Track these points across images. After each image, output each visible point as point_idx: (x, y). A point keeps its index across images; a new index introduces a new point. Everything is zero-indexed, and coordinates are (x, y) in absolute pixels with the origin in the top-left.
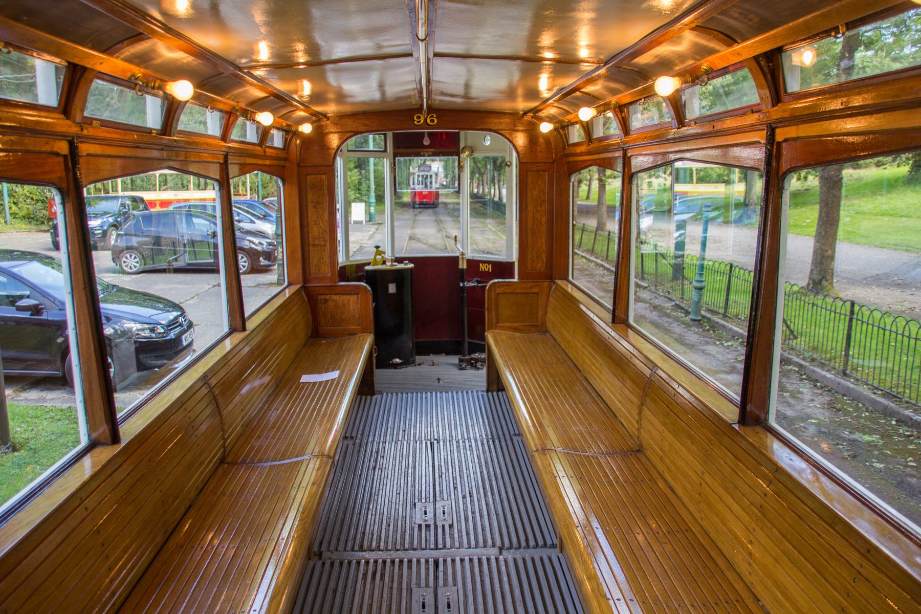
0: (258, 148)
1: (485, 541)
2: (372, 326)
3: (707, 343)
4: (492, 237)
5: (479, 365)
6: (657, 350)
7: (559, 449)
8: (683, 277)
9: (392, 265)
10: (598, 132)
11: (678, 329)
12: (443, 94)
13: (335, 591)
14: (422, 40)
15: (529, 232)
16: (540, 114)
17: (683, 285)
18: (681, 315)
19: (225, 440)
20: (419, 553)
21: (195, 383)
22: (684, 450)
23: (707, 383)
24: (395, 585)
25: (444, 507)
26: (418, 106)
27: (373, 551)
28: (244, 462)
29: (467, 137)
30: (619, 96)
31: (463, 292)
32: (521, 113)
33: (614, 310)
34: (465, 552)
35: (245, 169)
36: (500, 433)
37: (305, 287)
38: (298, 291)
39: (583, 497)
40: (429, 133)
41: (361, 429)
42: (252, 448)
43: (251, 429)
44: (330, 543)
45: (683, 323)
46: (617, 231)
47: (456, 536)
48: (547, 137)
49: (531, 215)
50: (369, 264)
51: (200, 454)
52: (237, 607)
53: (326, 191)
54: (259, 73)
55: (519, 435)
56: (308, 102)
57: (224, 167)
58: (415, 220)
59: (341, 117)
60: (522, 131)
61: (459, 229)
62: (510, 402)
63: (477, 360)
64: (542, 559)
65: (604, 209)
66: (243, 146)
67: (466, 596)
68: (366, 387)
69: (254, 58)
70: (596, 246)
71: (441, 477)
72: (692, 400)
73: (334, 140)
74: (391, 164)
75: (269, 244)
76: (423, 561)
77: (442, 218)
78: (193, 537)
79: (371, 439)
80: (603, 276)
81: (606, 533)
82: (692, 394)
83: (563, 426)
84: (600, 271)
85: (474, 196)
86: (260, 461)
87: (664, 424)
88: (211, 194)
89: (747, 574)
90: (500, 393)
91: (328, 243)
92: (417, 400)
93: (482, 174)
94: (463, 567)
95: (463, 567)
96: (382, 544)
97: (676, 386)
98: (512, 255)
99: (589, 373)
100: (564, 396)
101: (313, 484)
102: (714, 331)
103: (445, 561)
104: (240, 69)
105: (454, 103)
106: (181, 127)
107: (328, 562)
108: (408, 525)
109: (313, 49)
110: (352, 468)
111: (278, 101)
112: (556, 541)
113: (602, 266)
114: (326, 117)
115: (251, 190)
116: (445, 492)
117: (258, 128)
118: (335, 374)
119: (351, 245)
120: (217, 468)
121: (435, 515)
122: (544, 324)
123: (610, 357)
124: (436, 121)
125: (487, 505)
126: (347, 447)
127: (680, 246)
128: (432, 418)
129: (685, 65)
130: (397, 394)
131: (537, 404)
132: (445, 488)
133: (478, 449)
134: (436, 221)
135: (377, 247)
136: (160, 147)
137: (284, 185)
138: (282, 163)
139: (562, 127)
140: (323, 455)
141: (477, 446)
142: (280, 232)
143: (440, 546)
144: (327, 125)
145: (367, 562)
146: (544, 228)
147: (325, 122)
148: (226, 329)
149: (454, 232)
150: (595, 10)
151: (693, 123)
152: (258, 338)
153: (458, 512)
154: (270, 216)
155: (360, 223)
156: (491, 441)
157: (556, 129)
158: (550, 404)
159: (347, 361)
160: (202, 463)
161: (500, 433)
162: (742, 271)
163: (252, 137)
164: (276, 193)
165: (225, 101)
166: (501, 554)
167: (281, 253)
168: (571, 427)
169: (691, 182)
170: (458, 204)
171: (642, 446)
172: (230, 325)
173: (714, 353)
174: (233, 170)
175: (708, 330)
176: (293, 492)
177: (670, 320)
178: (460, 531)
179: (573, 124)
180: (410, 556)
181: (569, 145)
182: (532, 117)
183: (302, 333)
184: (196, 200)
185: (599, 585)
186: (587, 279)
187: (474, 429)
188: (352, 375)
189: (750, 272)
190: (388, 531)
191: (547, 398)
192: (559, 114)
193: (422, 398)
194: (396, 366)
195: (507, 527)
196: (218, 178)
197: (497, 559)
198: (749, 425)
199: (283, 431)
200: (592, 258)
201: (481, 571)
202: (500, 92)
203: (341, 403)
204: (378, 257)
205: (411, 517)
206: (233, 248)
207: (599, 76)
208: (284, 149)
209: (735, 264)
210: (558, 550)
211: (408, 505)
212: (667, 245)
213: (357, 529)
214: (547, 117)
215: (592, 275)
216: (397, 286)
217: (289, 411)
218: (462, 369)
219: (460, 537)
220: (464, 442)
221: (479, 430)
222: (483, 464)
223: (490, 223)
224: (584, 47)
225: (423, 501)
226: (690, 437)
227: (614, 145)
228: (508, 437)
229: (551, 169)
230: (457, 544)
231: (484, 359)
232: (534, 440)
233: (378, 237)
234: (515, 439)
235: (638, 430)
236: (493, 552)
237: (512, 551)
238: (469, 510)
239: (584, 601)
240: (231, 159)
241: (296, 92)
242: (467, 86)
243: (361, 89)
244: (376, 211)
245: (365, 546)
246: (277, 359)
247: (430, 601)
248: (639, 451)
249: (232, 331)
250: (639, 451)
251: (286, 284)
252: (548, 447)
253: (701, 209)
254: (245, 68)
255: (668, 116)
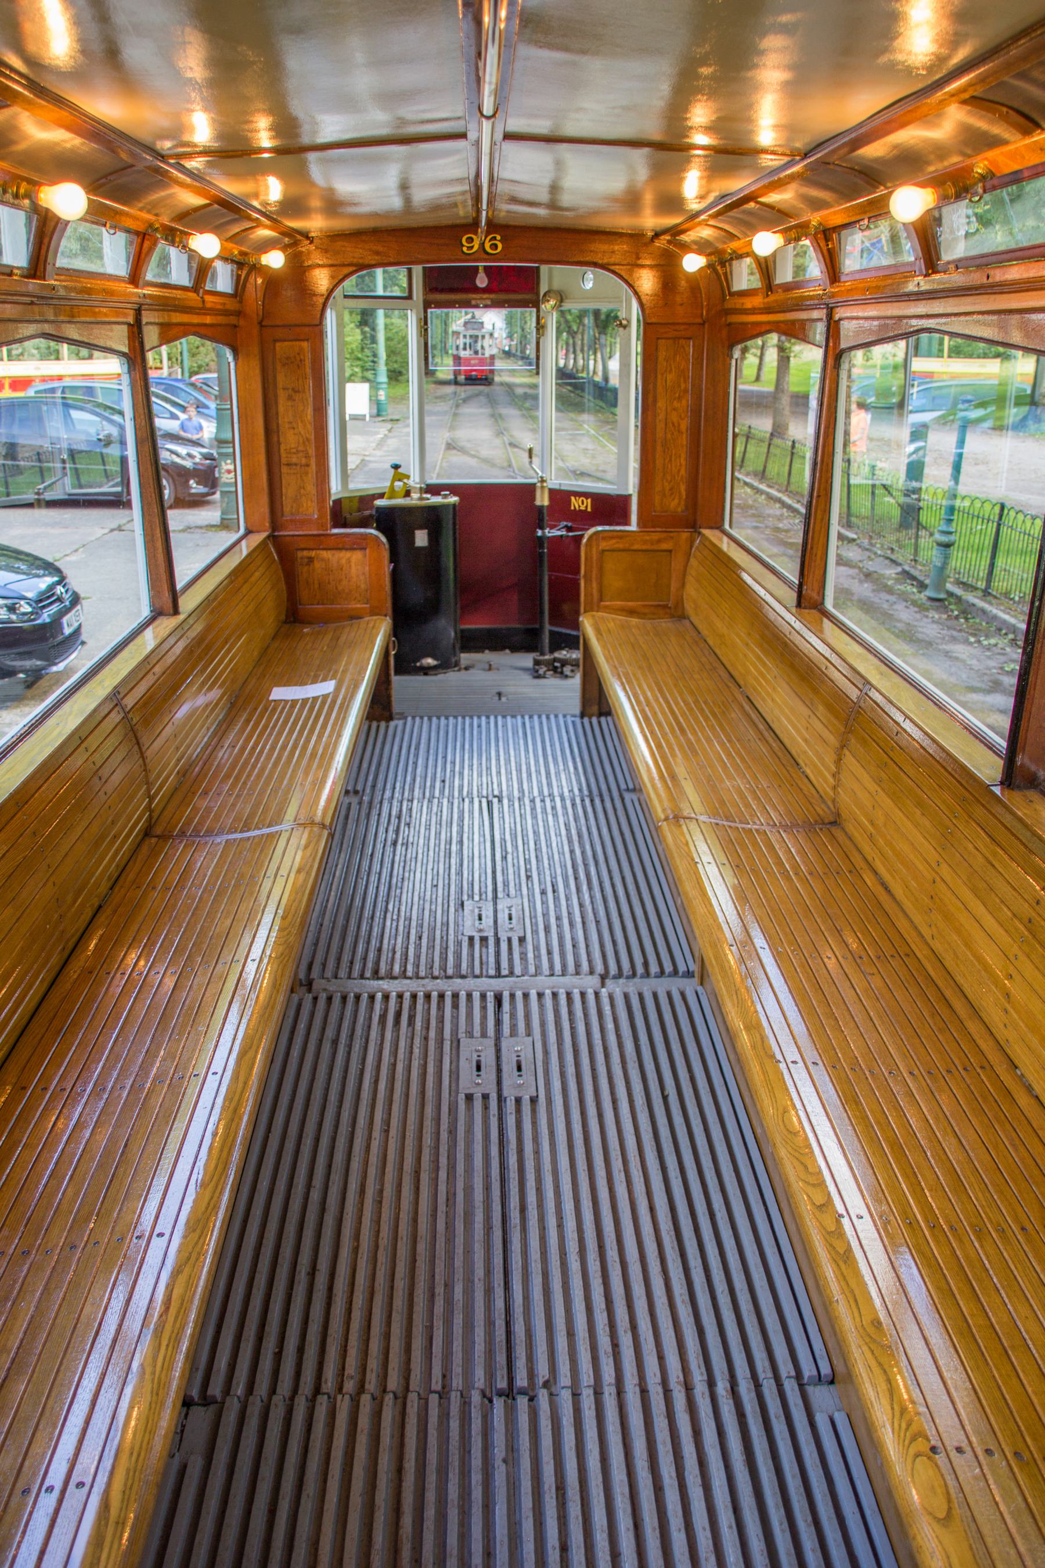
0: (192, 295)
1: (578, 965)
2: (389, 604)
3: (954, 639)
4: (590, 446)
5: (567, 670)
6: (871, 657)
7: (703, 818)
8: (919, 523)
9: (421, 499)
10: (784, 275)
11: (905, 614)
12: (514, 200)
13: (335, 1042)
14: (488, 118)
15: (659, 448)
16: (684, 238)
17: (917, 537)
18: (910, 588)
19: (152, 799)
20: (470, 983)
21: (99, 705)
22: (909, 823)
23: (952, 716)
24: (432, 1034)
25: (510, 908)
26: (470, 221)
27: (396, 978)
28: (183, 833)
29: (552, 276)
30: (824, 212)
31: (542, 546)
32: (650, 234)
33: (801, 585)
34: (545, 983)
35: (169, 334)
36: (604, 787)
37: (274, 536)
38: (263, 544)
39: (740, 896)
40: (485, 267)
41: (371, 778)
42: (195, 810)
43: (191, 781)
44: (324, 965)
45: (914, 603)
46: (810, 443)
47: (530, 955)
48: (693, 280)
49: (661, 416)
50: (381, 496)
51: (113, 822)
52: (186, 1068)
53: (308, 371)
54: (195, 164)
55: (634, 790)
56: (277, 213)
57: (136, 331)
58: (455, 415)
59: (335, 237)
60: (651, 267)
61: (534, 431)
62: (620, 735)
63: (564, 663)
64: (669, 995)
65: (785, 401)
66: (166, 293)
67: (546, 1052)
68: (380, 707)
69: (186, 138)
70: (769, 466)
71: (504, 858)
72: (927, 743)
73: (321, 279)
74: (419, 320)
75: (206, 457)
76: (476, 995)
77: (504, 411)
78: (106, 957)
79: (388, 794)
80: (780, 518)
81: (777, 956)
82: (926, 733)
83: (709, 779)
84: (776, 510)
85: (563, 374)
86: (209, 832)
87: (879, 781)
88: (109, 367)
89: (1001, 1026)
90: (603, 719)
91: (313, 462)
92: (463, 730)
93: (572, 334)
94: (541, 1006)
95: (541, 1006)
96: (410, 968)
97: (900, 718)
98: (626, 484)
99: (755, 689)
100: (712, 728)
101: (299, 871)
102: (966, 619)
103: (512, 996)
104: (163, 157)
105: (533, 215)
106: (61, 262)
107: (323, 996)
108: (451, 937)
109: (286, 126)
110: (358, 843)
111: (225, 213)
112: (693, 967)
113: (779, 501)
114: (308, 238)
115: (170, 359)
116: (512, 884)
117: (190, 259)
118: (327, 687)
119: (350, 459)
120: (139, 845)
121: (496, 922)
122: (680, 603)
123: (792, 666)
124: (500, 246)
125: (581, 905)
126: (349, 809)
127: (915, 470)
128: (489, 759)
129: (946, 163)
130: (430, 719)
131: (667, 742)
132: (511, 877)
133: (566, 814)
134: (493, 416)
135: (396, 467)
136: (27, 299)
137: (236, 358)
138: (233, 320)
139: (721, 262)
140: (313, 823)
141: (564, 807)
142: (228, 436)
143: (505, 972)
144: (309, 253)
145: (386, 997)
146: (684, 440)
147: (305, 247)
148: (146, 612)
149: (528, 440)
150: (790, 68)
151: (952, 267)
152: (199, 628)
153: (533, 917)
154: (207, 407)
155: (362, 418)
156: (587, 801)
157: (710, 266)
158: (688, 741)
159: (348, 663)
160: (116, 837)
161: (604, 787)
162: (1020, 517)
163: (179, 274)
164: (213, 365)
165: (137, 214)
166: (603, 985)
167: (230, 472)
168: (722, 781)
169: (940, 354)
170: (535, 386)
171: (839, 815)
172: (152, 604)
173: (963, 657)
174: (151, 335)
175: (957, 618)
176: (267, 884)
177: (893, 598)
178: (536, 948)
179: (740, 257)
180: (456, 988)
181: (732, 294)
182: (669, 242)
183: (271, 614)
184: (73, 376)
185: (763, 1038)
186: (757, 531)
187: (559, 780)
188: (356, 687)
189: (1034, 518)
190: (419, 946)
191: (683, 731)
192: (717, 239)
193: (471, 725)
194: (426, 671)
195: (614, 943)
196: (126, 350)
197: (597, 994)
198: (1019, 788)
199: (245, 783)
200: (763, 487)
201: (571, 1013)
202: (615, 200)
203: (339, 736)
204: (397, 484)
205: (456, 924)
206: (154, 468)
207: (792, 178)
208: (234, 295)
209: (1008, 505)
210: (696, 980)
211: (452, 904)
212: (893, 469)
213: (368, 942)
214: (695, 242)
215: (759, 516)
216: (429, 535)
217: (254, 748)
218: (539, 677)
219: (537, 957)
220: (543, 801)
221: (566, 781)
222: (575, 838)
223: (588, 422)
224: (767, 129)
225: (477, 898)
226: (920, 804)
227: (811, 298)
228: (615, 794)
229: (701, 329)
230: (532, 969)
231: (577, 660)
232: (660, 801)
233: (392, 443)
234: (628, 796)
235: (834, 788)
236: (590, 983)
237: (621, 981)
238: (552, 914)
239: (738, 1062)
240: (147, 317)
241: (256, 196)
242: (554, 189)
243: (371, 189)
244: (388, 397)
245: (383, 971)
246: (231, 661)
247: (488, 1059)
248: (834, 823)
249: (157, 614)
250: (834, 823)
251: (242, 531)
252: (685, 814)
253: (955, 404)
254: (171, 156)
255: (910, 253)
